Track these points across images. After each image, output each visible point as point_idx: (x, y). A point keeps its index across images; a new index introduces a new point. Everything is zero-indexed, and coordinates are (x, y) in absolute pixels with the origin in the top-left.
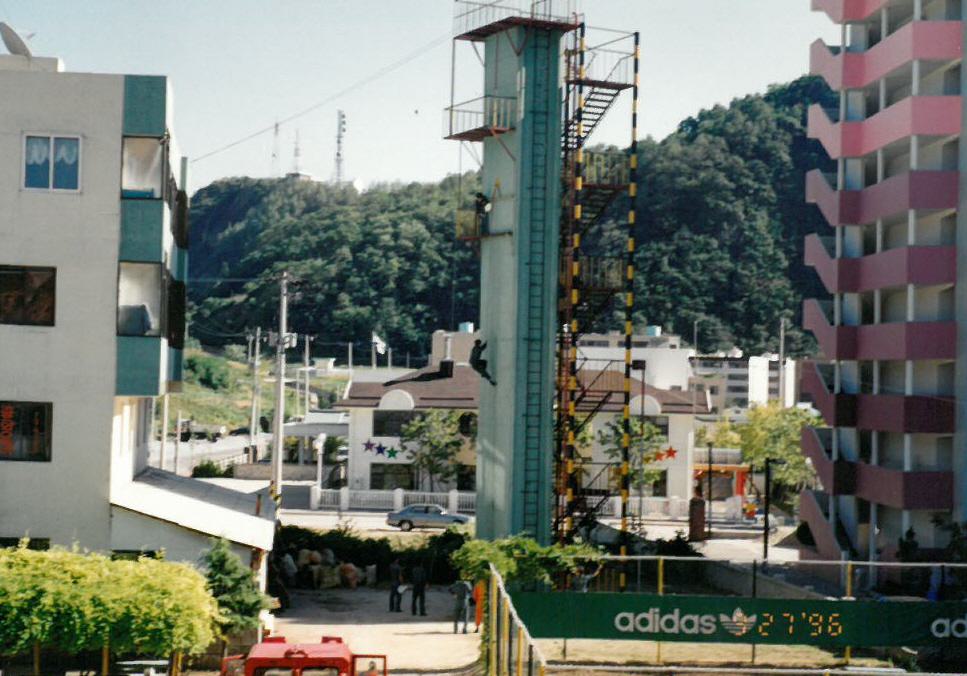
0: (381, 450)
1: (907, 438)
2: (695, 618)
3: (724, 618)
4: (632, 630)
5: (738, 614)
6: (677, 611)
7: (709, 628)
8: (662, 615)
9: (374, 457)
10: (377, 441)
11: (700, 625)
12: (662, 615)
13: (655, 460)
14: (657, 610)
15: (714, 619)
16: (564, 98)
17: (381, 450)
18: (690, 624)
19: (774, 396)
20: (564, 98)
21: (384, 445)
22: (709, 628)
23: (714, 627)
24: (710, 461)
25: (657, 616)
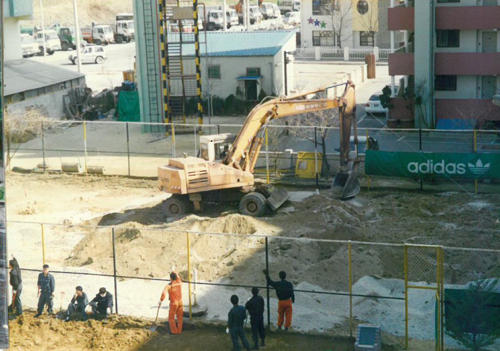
0: (317, 23)
1: (392, 33)
2: (454, 165)
3: (470, 165)
4: (417, 172)
5: (479, 163)
6: (443, 161)
7: (461, 171)
8: (434, 163)
9: (313, 27)
10: (315, 18)
11: (457, 169)
12: (434, 163)
13: (18, 143)
14: (432, 161)
15: (464, 166)
16: (444, 317)
17: (317, 23)
18: (451, 168)
19: (164, 189)
20: (444, 317)
21: (319, 20)
22: (461, 166)
23: (464, 170)
24: (149, 52)
25: (432, 165)
